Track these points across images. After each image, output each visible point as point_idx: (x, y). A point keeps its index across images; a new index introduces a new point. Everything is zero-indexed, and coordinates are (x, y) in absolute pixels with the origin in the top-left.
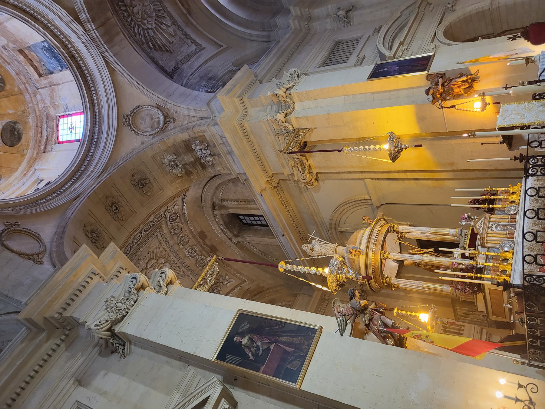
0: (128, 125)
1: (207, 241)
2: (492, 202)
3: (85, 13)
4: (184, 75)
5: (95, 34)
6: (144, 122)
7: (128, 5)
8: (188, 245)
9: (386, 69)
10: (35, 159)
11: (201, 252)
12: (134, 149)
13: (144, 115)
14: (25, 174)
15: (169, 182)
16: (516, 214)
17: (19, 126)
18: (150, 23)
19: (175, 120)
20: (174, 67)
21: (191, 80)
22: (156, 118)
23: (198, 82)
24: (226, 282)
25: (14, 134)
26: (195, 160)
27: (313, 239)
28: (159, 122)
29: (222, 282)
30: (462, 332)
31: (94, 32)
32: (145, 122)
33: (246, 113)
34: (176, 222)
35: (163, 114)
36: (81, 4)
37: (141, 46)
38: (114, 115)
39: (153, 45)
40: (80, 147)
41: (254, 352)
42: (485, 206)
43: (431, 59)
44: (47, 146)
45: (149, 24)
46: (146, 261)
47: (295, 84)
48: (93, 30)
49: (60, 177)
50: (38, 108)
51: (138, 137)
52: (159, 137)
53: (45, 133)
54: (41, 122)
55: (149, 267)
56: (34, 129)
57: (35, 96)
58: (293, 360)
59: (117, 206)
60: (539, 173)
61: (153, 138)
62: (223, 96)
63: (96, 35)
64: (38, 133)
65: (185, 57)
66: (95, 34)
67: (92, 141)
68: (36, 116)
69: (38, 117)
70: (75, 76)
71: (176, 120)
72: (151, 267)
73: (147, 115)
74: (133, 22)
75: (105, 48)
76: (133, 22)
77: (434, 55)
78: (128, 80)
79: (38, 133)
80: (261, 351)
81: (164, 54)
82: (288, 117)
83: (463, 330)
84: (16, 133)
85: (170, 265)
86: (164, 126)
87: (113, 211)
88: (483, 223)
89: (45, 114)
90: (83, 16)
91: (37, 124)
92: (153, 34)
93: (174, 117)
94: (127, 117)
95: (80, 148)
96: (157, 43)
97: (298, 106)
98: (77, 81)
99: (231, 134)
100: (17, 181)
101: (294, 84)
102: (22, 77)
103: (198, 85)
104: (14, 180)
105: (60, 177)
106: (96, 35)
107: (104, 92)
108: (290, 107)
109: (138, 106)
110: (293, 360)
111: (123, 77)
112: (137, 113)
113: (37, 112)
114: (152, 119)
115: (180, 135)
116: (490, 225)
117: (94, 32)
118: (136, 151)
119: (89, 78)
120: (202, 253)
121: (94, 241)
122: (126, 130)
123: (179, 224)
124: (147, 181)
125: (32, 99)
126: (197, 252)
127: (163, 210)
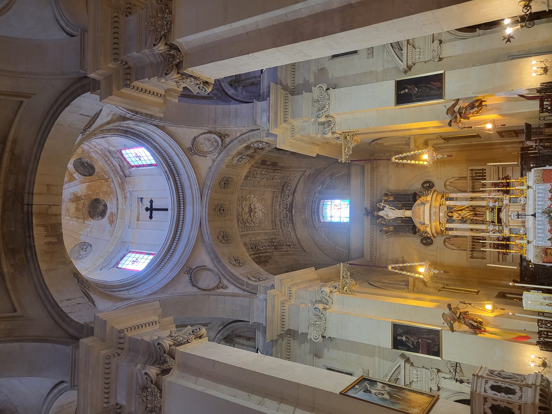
1: (268, 163)
2: (508, 185)
6: (204, 145)
9: (406, 90)
10: (123, 183)
11: (267, 172)
12: (210, 168)
16: (525, 204)
17: (85, 160)
19: (228, 136)
24: (293, 178)
27: (384, 207)
28: (216, 141)
29: (290, 180)
30: (485, 177)
32: (205, 145)
33: (293, 127)
35: (217, 135)
38: (181, 153)
41: (412, 344)
42: (504, 188)
43: (443, 76)
49: (173, 209)
50: (98, 149)
52: (224, 152)
53: (116, 163)
54: (107, 156)
55: (244, 207)
56: (105, 163)
58: (433, 347)
59: (222, 209)
60: (544, 327)
62: (274, 129)
67: (173, 173)
68: (100, 155)
69: (102, 154)
73: (204, 140)
77: (445, 72)
80: (415, 343)
83: (485, 176)
84: (86, 165)
88: (505, 214)
89: (106, 151)
93: (227, 133)
94: (190, 149)
97: (338, 119)
98: (138, 143)
100: (124, 205)
105: (173, 209)
108: (332, 122)
109: (195, 138)
110: (433, 347)
113: (99, 152)
114: (210, 141)
116: (510, 214)
122: (196, 158)
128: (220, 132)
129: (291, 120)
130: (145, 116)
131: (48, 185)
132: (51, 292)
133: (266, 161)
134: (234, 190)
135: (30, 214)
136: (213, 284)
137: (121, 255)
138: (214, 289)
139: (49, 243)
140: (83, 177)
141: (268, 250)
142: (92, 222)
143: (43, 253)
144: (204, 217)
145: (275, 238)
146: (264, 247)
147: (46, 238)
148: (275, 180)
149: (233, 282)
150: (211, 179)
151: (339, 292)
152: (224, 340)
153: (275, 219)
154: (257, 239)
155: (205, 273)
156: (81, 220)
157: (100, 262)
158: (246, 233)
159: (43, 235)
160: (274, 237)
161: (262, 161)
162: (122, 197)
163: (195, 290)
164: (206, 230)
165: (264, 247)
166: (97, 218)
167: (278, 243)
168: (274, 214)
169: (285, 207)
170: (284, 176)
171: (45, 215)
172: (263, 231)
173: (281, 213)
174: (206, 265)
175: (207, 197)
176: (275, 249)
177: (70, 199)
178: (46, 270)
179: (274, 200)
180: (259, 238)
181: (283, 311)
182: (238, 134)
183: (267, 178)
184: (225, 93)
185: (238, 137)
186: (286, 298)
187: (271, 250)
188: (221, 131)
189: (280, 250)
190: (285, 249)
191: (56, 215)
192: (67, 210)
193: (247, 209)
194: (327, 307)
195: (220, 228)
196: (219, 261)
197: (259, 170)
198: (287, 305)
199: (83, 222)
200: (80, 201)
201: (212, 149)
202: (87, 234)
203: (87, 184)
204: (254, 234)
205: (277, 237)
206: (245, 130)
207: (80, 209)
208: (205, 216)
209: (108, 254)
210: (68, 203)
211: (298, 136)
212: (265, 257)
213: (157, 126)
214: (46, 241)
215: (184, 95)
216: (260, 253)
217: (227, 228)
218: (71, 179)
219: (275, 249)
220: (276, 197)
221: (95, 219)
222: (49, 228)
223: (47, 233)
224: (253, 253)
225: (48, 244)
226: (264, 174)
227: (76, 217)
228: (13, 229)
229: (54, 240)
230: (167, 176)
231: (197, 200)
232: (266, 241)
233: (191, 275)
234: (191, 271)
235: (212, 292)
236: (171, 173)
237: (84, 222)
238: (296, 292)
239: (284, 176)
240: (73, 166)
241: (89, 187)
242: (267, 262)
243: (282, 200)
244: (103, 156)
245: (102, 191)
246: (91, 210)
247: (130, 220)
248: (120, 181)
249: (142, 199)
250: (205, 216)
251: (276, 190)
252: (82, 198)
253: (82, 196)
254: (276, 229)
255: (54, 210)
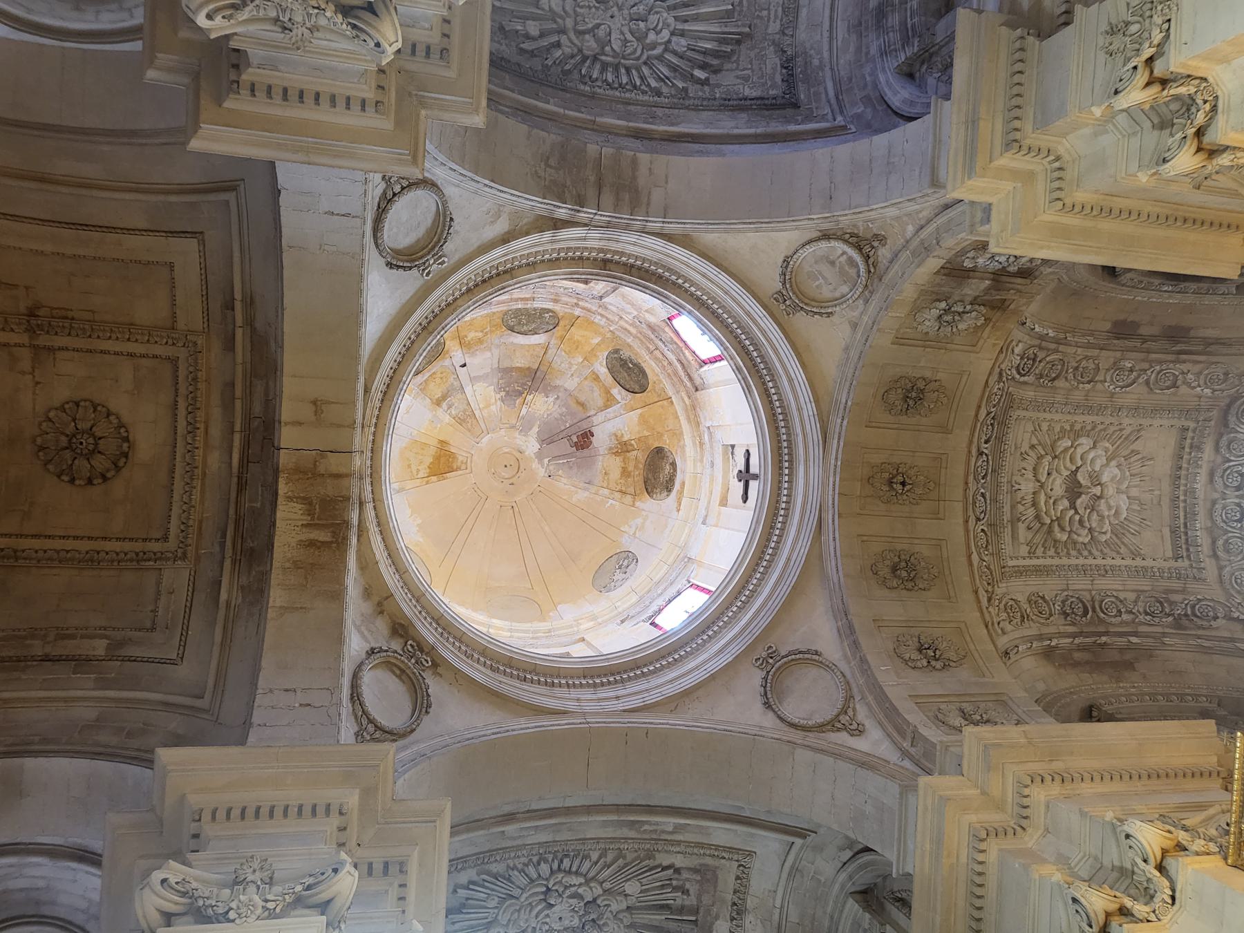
0: (797, 308)
1: (1144, 331)
3: (560, 207)
4: (816, 62)
5: (604, 216)
6: (821, 281)
7: (597, 51)
8: (1102, 372)
12: (847, 349)
13: (810, 266)
14: (701, 444)
15: (970, 348)
17: (625, 354)
18: (659, 27)
19: (882, 239)
20: (783, 67)
21: (842, 61)
22: (839, 257)
23: (859, 49)
25: (629, 368)
26: (993, 280)
28: (851, 261)
31: (601, 215)
32: (824, 277)
33: (1057, 164)
34: (1040, 361)
35: (846, 241)
36: (542, 203)
37: (687, 103)
39: (704, 67)
40: (748, 396)
44: (692, 375)
45: (661, 30)
46: (1030, 475)
47: (1169, 20)
48: (596, 214)
50: (626, 322)
51: (834, 319)
52: (878, 295)
57: (606, 308)
59: (900, 478)
61: (867, 301)
63: (607, 216)
64: (660, 362)
65: (784, 11)
66: (603, 217)
69: (639, 335)
70: (637, 287)
71: (883, 236)
72: (1049, 474)
73: (816, 262)
74: (634, 71)
75: (640, 220)
76: (634, 71)
78: (726, 231)
79: (660, 362)
81: (738, 58)
82: (1207, 139)
85: (1088, 436)
86: (868, 265)
87: (902, 493)
89: (644, 326)
90: (562, 212)
91: (648, 348)
92: (683, 42)
93: (875, 231)
94: (781, 297)
95: (750, 399)
96: (705, 52)
98: (647, 291)
99: (1053, 244)
101: (1166, 26)
102: (565, 299)
103: (864, 59)
104: (695, 466)
106: (607, 216)
107: (704, 280)
108: (1200, 102)
109: (786, 261)
111: (711, 237)
112: (794, 274)
114: (832, 263)
115: (922, 270)
117: (601, 215)
118: (854, 354)
119: (660, 271)
120: (1151, 362)
121: (910, 585)
122: (801, 321)
123: (1048, 359)
124: (921, 384)
125: (607, 318)
126: (1137, 368)
127: (995, 377)
128: (856, 232)
129: (1032, 137)
130: (612, 210)
131: (314, 403)
132: (264, 663)
133: (1135, 325)
134: (951, 420)
135: (276, 472)
136: (825, 713)
137: (672, 591)
138: (821, 728)
139: (312, 544)
140: (630, 395)
141: (1142, 629)
142: (648, 504)
143: (287, 565)
144: (830, 502)
145: (1183, 591)
146: (1125, 617)
147: (304, 530)
148: (1184, 390)
149: (677, 727)
150: (848, 384)
151: (1225, 859)
152: (858, 897)
153: (1185, 525)
154: (1096, 587)
155: (813, 672)
156: (628, 499)
157: (629, 603)
158: (1048, 562)
159: (300, 523)
160: (1176, 585)
161: (1116, 324)
162: (694, 443)
163: (769, 720)
164: (832, 542)
165: (1125, 617)
166: (658, 494)
167: (1193, 607)
168: (1182, 505)
169: (1236, 484)
170: (1226, 374)
171: (310, 476)
172: (1128, 562)
173: (1214, 502)
174: (819, 649)
175: (838, 442)
176: (1175, 629)
177: (611, 449)
178: (281, 607)
179: (1186, 457)
180: (1104, 584)
181: (979, 868)
182: (910, 229)
183: (1147, 383)
184: (885, 106)
185: (911, 239)
186: (995, 818)
187: (1159, 629)
188: (854, 226)
189: (1200, 632)
190: (1226, 634)
191: (338, 476)
192: (605, 473)
193: (1058, 486)
194: (1140, 909)
195: (889, 539)
196: (856, 645)
197: (1106, 358)
198: (993, 849)
199: (632, 503)
200: (629, 452)
201: (845, 289)
202: (635, 533)
203: (639, 411)
204: (1084, 570)
205: (1192, 586)
206: (925, 213)
207: (630, 473)
208: (834, 499)
209: (651, 585)
210: (608, 456)
211: (1080, 196)
212: (1121, 650)
213: (669, 238)
214: (303, 539)
215: (760, 135)
216: (1106, 633)
217: (916, 541)
218: (608, 400)
219: (1177, 624)
220: (1191, 447)
221: (654, 496)
222: (317, 506)
223: (309, 518)
224: (1071, 629)
225: (308, 546)
226: (1131, 370)
227: (621, 491)
228: (259, 505)
229: (324, 536)
230: (742, 382)
231: (816, 451)
232: (1138, 597)
233: (768, 672)
234: (771, 661)
235: (812, 739)
236: (753, 371)
237: (634, 502)
238: (1047, 807)
239: (1226, 374)
240: (606, 370)
241: (643, 420)
242: (1130, 666)
243: (1219, 460)
244: (642, 338)
245: (667, 429)
246: (650, 476)
247: (709, 502)
248: (687, 403)
249: (733, 446)
250: (834, 499)
251: (1192, 425)
252: (632, 445)
253: (633, 442)
254: (1189, 557)
255: (333, 463)
